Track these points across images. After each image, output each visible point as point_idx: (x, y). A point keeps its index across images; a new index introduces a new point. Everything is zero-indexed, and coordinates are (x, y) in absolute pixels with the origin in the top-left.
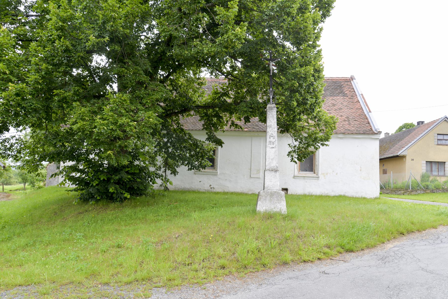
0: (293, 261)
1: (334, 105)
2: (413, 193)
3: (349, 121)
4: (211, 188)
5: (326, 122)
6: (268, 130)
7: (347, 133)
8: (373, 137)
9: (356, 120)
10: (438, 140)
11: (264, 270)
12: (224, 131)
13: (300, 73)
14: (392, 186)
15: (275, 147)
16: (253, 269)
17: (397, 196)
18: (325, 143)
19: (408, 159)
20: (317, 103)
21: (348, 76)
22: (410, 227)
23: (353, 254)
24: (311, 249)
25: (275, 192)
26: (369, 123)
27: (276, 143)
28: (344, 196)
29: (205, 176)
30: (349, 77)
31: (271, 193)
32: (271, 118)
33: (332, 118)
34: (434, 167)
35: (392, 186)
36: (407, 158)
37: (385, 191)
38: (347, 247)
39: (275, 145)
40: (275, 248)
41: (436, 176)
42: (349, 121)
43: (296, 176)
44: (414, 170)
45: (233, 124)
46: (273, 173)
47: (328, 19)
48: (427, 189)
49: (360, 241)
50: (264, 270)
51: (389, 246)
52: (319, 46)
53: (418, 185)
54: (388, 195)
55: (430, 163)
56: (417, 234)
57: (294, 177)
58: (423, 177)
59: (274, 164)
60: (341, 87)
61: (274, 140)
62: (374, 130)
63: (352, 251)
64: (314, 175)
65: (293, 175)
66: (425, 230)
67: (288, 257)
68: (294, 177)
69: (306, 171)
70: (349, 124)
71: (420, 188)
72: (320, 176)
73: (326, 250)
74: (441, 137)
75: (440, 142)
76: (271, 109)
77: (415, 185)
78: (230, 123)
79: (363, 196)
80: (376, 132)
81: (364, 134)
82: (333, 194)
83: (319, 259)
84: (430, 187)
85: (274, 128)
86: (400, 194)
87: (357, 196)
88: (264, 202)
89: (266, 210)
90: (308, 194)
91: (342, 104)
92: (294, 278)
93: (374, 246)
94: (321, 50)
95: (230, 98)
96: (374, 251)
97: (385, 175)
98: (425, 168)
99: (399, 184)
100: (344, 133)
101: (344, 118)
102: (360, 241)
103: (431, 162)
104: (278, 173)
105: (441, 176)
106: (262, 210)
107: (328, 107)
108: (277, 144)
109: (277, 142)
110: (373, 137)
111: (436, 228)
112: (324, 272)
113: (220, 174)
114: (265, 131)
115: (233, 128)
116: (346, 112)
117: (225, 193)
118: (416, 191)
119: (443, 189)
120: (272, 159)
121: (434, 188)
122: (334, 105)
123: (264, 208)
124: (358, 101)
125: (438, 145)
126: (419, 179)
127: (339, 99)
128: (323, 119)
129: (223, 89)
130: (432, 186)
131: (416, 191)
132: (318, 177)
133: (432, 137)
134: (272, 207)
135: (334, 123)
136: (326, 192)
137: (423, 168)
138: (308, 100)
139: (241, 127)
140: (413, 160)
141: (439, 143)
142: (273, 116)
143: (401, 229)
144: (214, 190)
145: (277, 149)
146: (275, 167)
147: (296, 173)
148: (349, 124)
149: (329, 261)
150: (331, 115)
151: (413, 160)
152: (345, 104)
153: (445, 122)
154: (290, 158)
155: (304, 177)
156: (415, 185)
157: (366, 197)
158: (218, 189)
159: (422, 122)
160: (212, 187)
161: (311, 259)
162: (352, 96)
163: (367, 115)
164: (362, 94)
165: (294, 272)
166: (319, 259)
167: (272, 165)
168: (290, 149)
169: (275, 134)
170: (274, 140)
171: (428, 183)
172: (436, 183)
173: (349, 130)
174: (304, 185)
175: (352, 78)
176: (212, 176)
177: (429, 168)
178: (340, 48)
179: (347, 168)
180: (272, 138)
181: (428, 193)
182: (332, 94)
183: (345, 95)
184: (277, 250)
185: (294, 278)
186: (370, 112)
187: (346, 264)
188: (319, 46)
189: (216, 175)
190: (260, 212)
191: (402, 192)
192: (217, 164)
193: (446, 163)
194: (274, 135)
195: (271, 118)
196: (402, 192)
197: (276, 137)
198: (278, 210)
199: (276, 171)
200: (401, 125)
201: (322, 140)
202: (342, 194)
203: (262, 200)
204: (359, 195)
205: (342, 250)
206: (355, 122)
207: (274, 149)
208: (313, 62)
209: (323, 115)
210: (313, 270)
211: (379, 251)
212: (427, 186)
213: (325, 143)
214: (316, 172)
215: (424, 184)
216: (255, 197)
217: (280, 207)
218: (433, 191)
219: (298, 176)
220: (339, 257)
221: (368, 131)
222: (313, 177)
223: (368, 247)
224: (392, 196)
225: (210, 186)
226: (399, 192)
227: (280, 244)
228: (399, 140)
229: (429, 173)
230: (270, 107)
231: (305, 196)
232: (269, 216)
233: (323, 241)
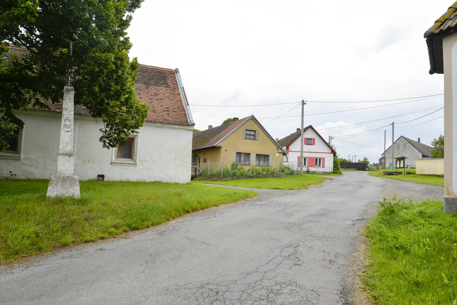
0: (73, 242)
1: (156, 95)
2: (223, 179)
3: (168, 111)
4: (12, 175)
5: (138, 110)
6: (64, 112)
7: (165, 123)
8: (188, 128)
9: (174, 112)
10: (246, 134)
11: (38, 254)
12: (27, 110)
13: (101, 58)
14: (209, 173)
15: (71, 131)
16: (27, 253)
17: (211, 182)
18: (136, 130)
19: (223, 150)
20: (123, 90)
21: (173, 67)
22: (195, 205)
23: (137, 232)
24: (96, 229)
25: (68, 177)
26: (185, 115)
27: (72, 127)
28: (160, 182)
29: (3, 160)
30: (174, 69)
31: (63, 178)
32: (67, 101)
33: (144, 106)
34: (262, 159)
35: (209, 173)
36: (222, 148)
37: (203, 178)
38: (133, 226)
39: (70, 129)
40: (57, 231)
41: (243, 165)
42: (168, 111)
43: (113, 163)
44: (226, 160)
45: (37, 102)
46: (67, 157)
47: (137, 10)
48: (234, 175)
49: (148, 219)
50: (38, 254)
51: (173, 222)
52: (126, 34)
53: (228, 172)
54: (205, 182)
55: (239, 154)
56: (201, 212)
57: (112, 163)
58: (234, 166)
59: (69, 148)
60: (165, 78)
61: (70, 124)
62: (189, 121)
63: (137, 229)
64: (132, 162)
65: (110, 162)
66: (208, 208)
67: (69, 238)
68: (112, 163)
69: (125, 157)
70: (168, 114)
71: (230, 175)
72: (137, 163)
73: (113, 230)
74: (248, 133)
75: (247, 137)
76: (69, 91)
77: (226, 172)
78: (33, 101)
79: (177, 182)
80: (190, 124)
81: (180, 125)
82: (148, 180)
83: (102, 238)
84: (237, 174)
85: (71, 112)
86: (214, 181)
87: (172, 182)
88: (55, 187)
89: (57, 195)
90: (124, 180)
91: (164, 94)
92: (68, 257)
93: (159, 224)
94: (128, 38)
95: (34, 72)
96: (158, 228)
97: (205, 163)
98: (235, 158)
99: (215, 172)
100: (162, 123)
101: (164, 108)
102: (148, 219)
103: (240, 153)
104: (72, 158)
105: (246, 165)
106: (52, 195)
107: (140, 96)
108: (73, 128)
109: (73, 125)
110: (188, 128)
111: (218, 206)
112: (101, 249)
113: (24, 159)
114: (61, 113)
115: (37, 107)
116: (167, 103)
117: (29, 180)
118: (226, 178)
119: (246, 175)
120: (67, 143)
121: (239, 175)
122: (156, 95)
123: (55, 193)
124: (179, 94)
125: (246, 139)
126: (229, 167)
127: (162, 90)
128: (135, 107)
129: (25, 61)
130: (238, 173)
131: (226, 178)
132: (136, 164)
133: (242, 132)
134: (64, 192)
135: (146, 111)
136: (143, 179)
137: (233, 158)
138: (112, 87)
139: (48, 107)
140: (226, 151)
141: (247, 137)
142: (70, 99)
143: (188, 208)
144: (16, 177)
145: (73, 133)
146: (70, 152)
147: (114, 159)
148: (168, 114)
149: (112, 239)
150: (143, 104)
151: (226, 151)
152: (167, 95)
153: (252, 120)
154: (102, 143)
155: (122, 163)
156: (226, 172)
157: (179, 182)
158: (20, 175)
159: (237, 119)
160: (13, 173)
161: (93, 239)
162: (174, 88)
163: (185, 108)
164: (183, 88)
165: (71, 252)
166: (102, 238)
167: (67, 149)
168: (101, 134)
169: (72, 118)
170: (69, 124)
171: (236, 171)
172: (242, 170)
173: (167, 120)
174: (117, 170)
175: (177, 71)
176: (13, 161)
177: (238, 159)
178: (148, 39)
179: (162, 156)
180: (67, 121)
181: (235, 179)
182: (156, 84)
183: (168, 86)
184: (59, 234)
185: (68, 257)
186: (188, 105)
187: (127, 240)
188: (126, 34)
189: (18, 159)
190: (49, 198)
191: (216, 178)
192: (21, 148)
193: (251, 155)
194: (70, 118)
195: (67, 101)
196: (216, 178)
197: (72, 121)
198: (71, 195)
199: (70, 155)
200: (226, 120)
201: (132, 127)
202: (158, 180)
203: (52, 185)
204: (173, 181)
205: (128, 229)
206: (174, 113)
207: (69, 133)
208: (116, 49)
209: (134, 103)
210: (91, 249)
211: (161, 228)
212: (235, 173)
213: (136, 130)
214: (134, 159)
215: (232, 171)
216: (46, 182)
217: (72, 192)
218: (238, 178)
219: (116, 163)
220: (124, 235)
221: (184, 122)
222: (131, 164)
223: (153, 225)
224: (208, 182)
225: (11, 172)
226: (214, 179)
227: (63, 227)
228: (218, 133)
229: (238, 163)
230: (67, 89)
231: (121, 182)
232: (59, 201)
233: (110, 221)
